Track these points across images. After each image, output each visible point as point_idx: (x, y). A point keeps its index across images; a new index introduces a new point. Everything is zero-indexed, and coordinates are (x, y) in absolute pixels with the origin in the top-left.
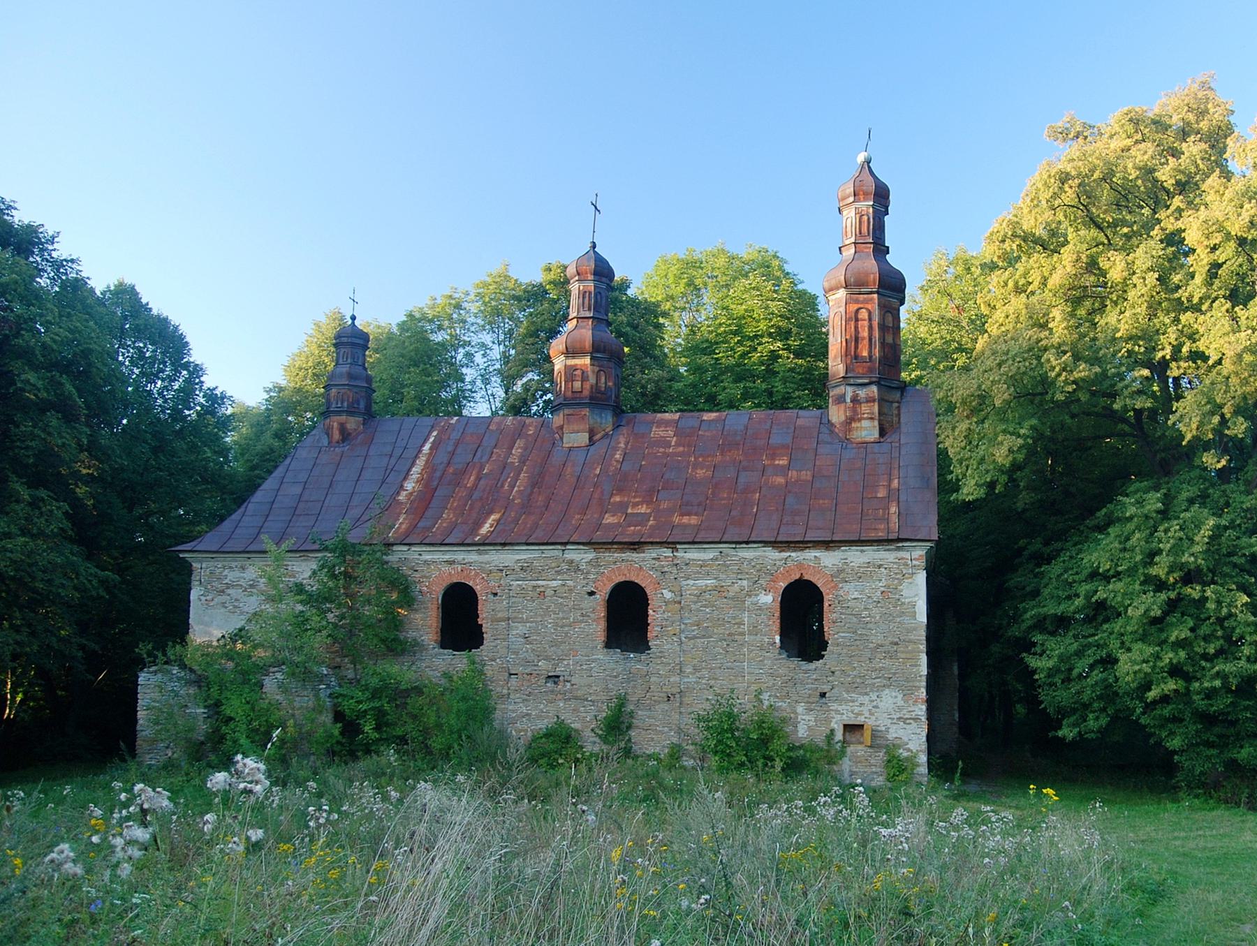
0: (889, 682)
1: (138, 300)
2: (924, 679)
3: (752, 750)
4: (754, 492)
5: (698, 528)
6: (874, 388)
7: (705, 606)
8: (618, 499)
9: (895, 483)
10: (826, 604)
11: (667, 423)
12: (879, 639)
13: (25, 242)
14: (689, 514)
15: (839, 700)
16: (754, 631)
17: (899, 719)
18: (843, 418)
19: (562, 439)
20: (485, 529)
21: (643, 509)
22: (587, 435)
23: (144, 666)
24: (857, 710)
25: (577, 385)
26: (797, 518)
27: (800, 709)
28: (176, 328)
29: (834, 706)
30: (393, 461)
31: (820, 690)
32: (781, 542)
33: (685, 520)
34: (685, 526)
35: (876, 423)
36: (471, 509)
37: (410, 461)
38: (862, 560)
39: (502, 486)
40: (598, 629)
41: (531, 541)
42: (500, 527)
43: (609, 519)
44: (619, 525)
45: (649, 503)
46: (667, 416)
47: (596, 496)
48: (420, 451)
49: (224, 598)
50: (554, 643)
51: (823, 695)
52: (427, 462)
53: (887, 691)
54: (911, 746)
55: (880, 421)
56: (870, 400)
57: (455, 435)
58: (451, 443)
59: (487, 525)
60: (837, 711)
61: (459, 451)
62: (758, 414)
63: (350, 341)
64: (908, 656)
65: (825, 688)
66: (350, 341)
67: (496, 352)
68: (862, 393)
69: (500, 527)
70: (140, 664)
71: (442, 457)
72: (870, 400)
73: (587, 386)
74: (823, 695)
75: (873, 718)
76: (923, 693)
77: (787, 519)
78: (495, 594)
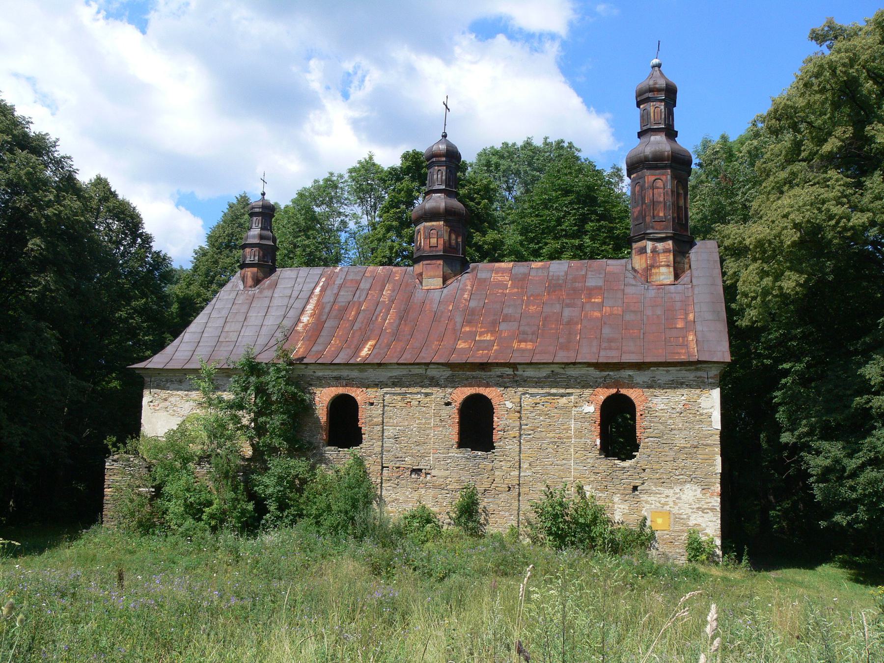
0: (692, 480)
1: (110, 189)
2: (719, 476)
3: (573, 529)
4: (577, 324)
5: (533, 352)
6: (670, 242)
7: (540, 415)
8: (468, 329)
9: (691, 317)
10: (638, 414)
11: (503, 271)
12: (681, 443)
13: (38, 147)
14: (525, 341)
15: (646, 492)
16: (579, 433)
17: (698, 508)
18: (644, 266)
19: (421, 283)
20: (365, 352)
21: (488, 337)
22: (441, 280)
23: (110, 454)
24: (663, 500)
25: (434, 241)
26: (612, 344)
27: (616, 499)
28: (134, 208)
29: (644, 497)
30: (292, 301)
31: (632, 484)
32: (580, 363)
33: (523, 345)
34: (523, 351)
35: (672, 269)
36: (353, 337)
37: (305, 301)
39: (377, 319)
40: (452, 432)
41: (401, 361)
42: (375, 351)
43: (461, 345)
44: (470, 349)
45: (493, 333)
46: (503, 265)
47: (450, 327)
48: (312, 293)
49: (167, 403)
50: (418, 444)
52: (318, 301)
53: (688, 486)
54: (708, 531)
55: (674, 267)
56: (666, 251)
57: (339, 281)
58: (336, 287)
59: (366, 349)
60: (647, 502)
61: (342, 293)
62: (575, 263)
65: (637, 482)
67: (365, 221)
68: (660, 246)
69: (375, 351)
70: (106, 453)
71: (329, 297)
72: (666, 251)
74: (635, 488)
75: (677, 508)
76: (718, 488)
77: (604, 345)
78: (372, 404)
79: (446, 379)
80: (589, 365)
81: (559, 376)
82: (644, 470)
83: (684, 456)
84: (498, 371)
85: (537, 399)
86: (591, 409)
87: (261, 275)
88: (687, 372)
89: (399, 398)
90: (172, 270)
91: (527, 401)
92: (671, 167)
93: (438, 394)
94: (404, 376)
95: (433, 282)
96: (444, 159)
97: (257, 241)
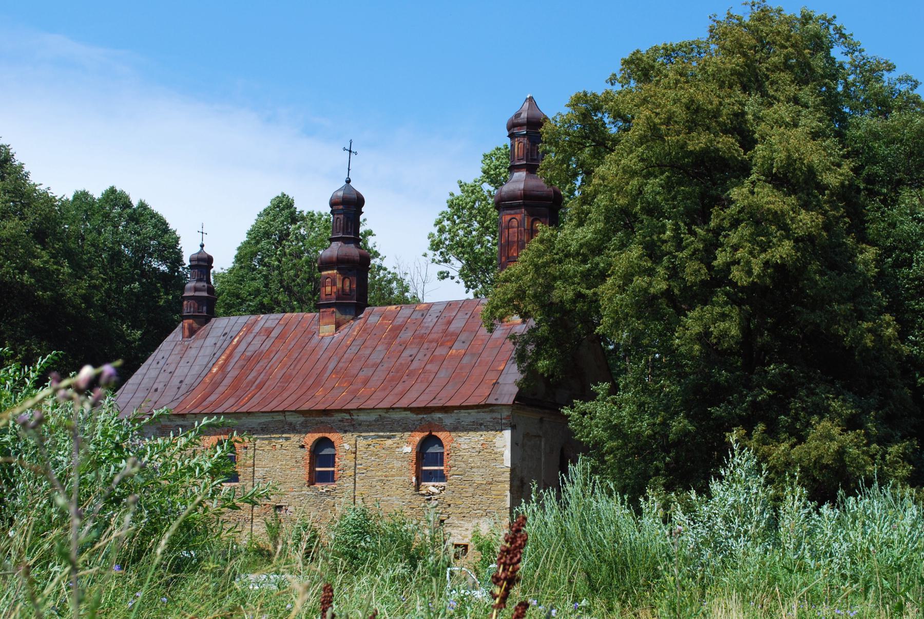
7: (371, 455)
12: (478, 480)
29: (448, 530)
38: (469, 420)
51: (442, 521)
63: (529, 128)
64: (499, 493)
65: (444, 517)
66: (529, 128)
73: (335, 290)
74: (442, 521)
79: (301, 424)
80: (405, 409)
81: (385, 422)
82: (449, 505)
83: (480, 492)
84: (339, 416)
85: (369, 441)
86: (408, 449)
87: (195, 325)
88: (483, 416)
89: (267, 442)
90: (524, 190)
91: (362, 443)
92: (524, 205)
93: (295, 438)
94: (269, 422)
95: (327, 329)
96: (341, 207)
97: (192, 294)
